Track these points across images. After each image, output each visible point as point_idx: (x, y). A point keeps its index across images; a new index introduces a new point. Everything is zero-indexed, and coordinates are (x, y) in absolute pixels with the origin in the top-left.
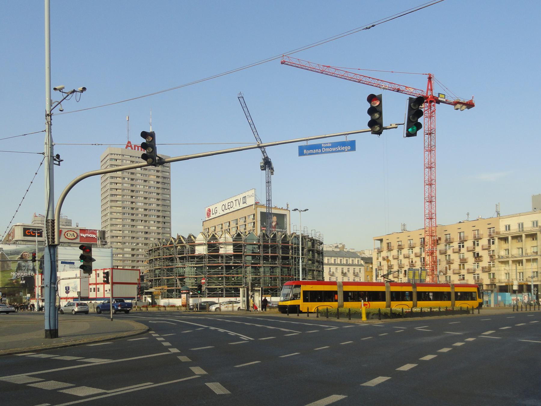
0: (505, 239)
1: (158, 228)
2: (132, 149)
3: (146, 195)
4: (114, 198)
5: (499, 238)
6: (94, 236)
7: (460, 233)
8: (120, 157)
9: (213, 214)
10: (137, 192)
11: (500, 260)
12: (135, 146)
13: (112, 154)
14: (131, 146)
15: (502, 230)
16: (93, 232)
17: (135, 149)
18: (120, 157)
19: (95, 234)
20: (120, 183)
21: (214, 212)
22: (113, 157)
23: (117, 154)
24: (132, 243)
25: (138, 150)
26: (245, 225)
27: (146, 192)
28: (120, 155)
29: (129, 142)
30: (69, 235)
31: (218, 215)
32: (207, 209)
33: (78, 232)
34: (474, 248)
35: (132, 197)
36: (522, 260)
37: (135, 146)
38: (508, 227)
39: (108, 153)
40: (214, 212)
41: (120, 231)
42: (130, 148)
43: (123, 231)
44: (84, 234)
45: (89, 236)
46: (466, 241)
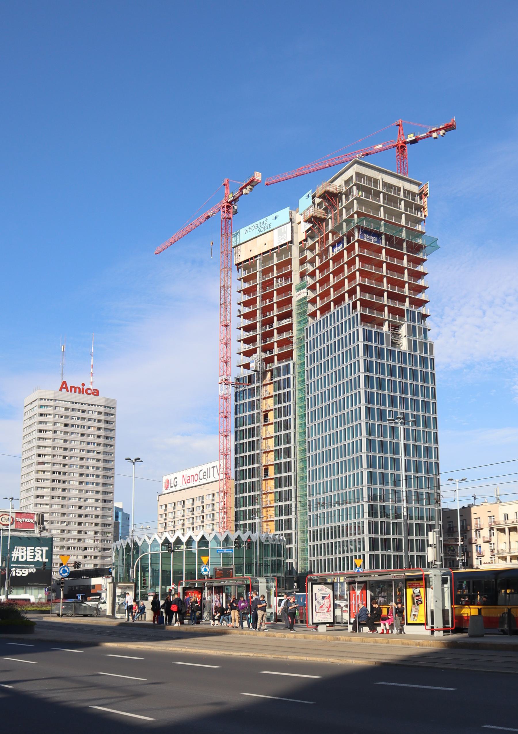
0: (503, 530)
1: (97, 500)
2: (67, 391)
3: (84, 454)
4: (41, 459)
5: (498, 530)
6: (32, 521)
7: (449, 522)
8: (51, 403)
9: (172, 487)
10: (71, 450)
11: (499, 556)
12: (71, 387)
13: (41, 399)
14: (66, 388)
15: (500, 519)
16: (29, 515)
17: (71, 391)
18: (51, 403)
19: (33, 518)
20: (50, 439)
21: (172, 485)
22: (43, 403)
23: (48, 400)
24: (62, 522)
25: (75, 392)
26: (214, 504)
27: (83, 450)
28: (51, 400)
29: (64, 383)
30: (3, 519)
31: (178, 488)
32: (164, 479)
33: (14, 515)
34: (490, 539)
35: (64, 457)
36: (506, 557)
37: (71, 387)
38: (507, 517)
39: (38, 397)
40: (172, 485)
41: (47, 504)
42: (64, 390)
43: (51, 505)
44: (21, 518)
45: (26, 520)
46: (482, 529)
